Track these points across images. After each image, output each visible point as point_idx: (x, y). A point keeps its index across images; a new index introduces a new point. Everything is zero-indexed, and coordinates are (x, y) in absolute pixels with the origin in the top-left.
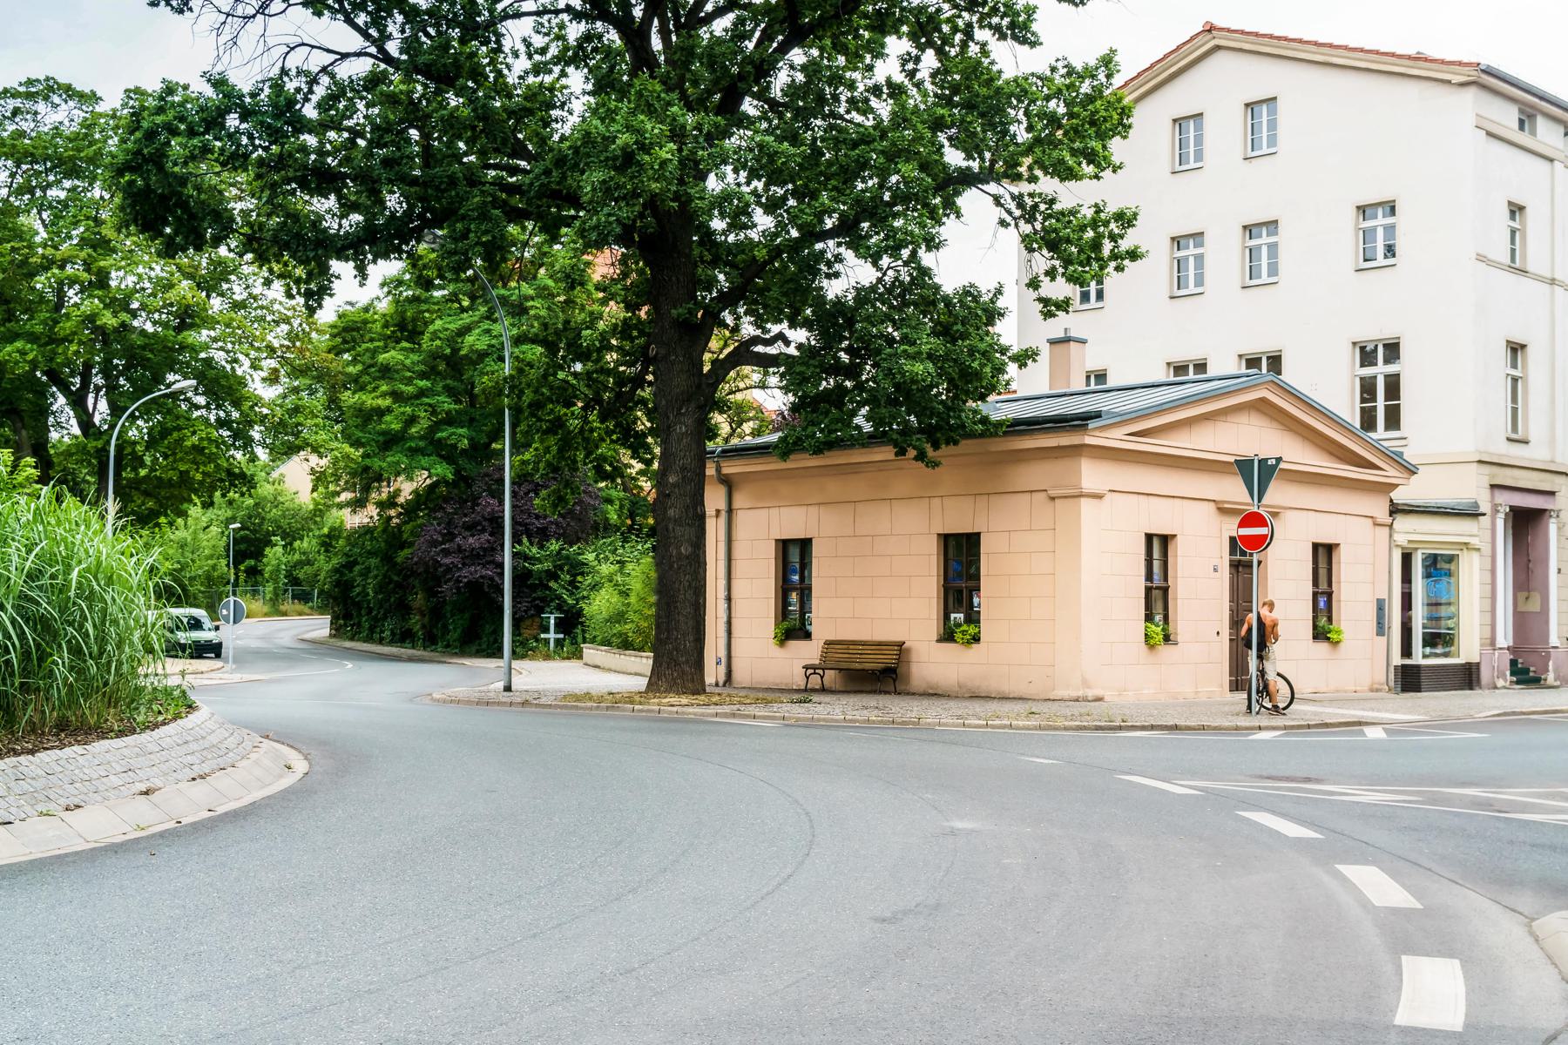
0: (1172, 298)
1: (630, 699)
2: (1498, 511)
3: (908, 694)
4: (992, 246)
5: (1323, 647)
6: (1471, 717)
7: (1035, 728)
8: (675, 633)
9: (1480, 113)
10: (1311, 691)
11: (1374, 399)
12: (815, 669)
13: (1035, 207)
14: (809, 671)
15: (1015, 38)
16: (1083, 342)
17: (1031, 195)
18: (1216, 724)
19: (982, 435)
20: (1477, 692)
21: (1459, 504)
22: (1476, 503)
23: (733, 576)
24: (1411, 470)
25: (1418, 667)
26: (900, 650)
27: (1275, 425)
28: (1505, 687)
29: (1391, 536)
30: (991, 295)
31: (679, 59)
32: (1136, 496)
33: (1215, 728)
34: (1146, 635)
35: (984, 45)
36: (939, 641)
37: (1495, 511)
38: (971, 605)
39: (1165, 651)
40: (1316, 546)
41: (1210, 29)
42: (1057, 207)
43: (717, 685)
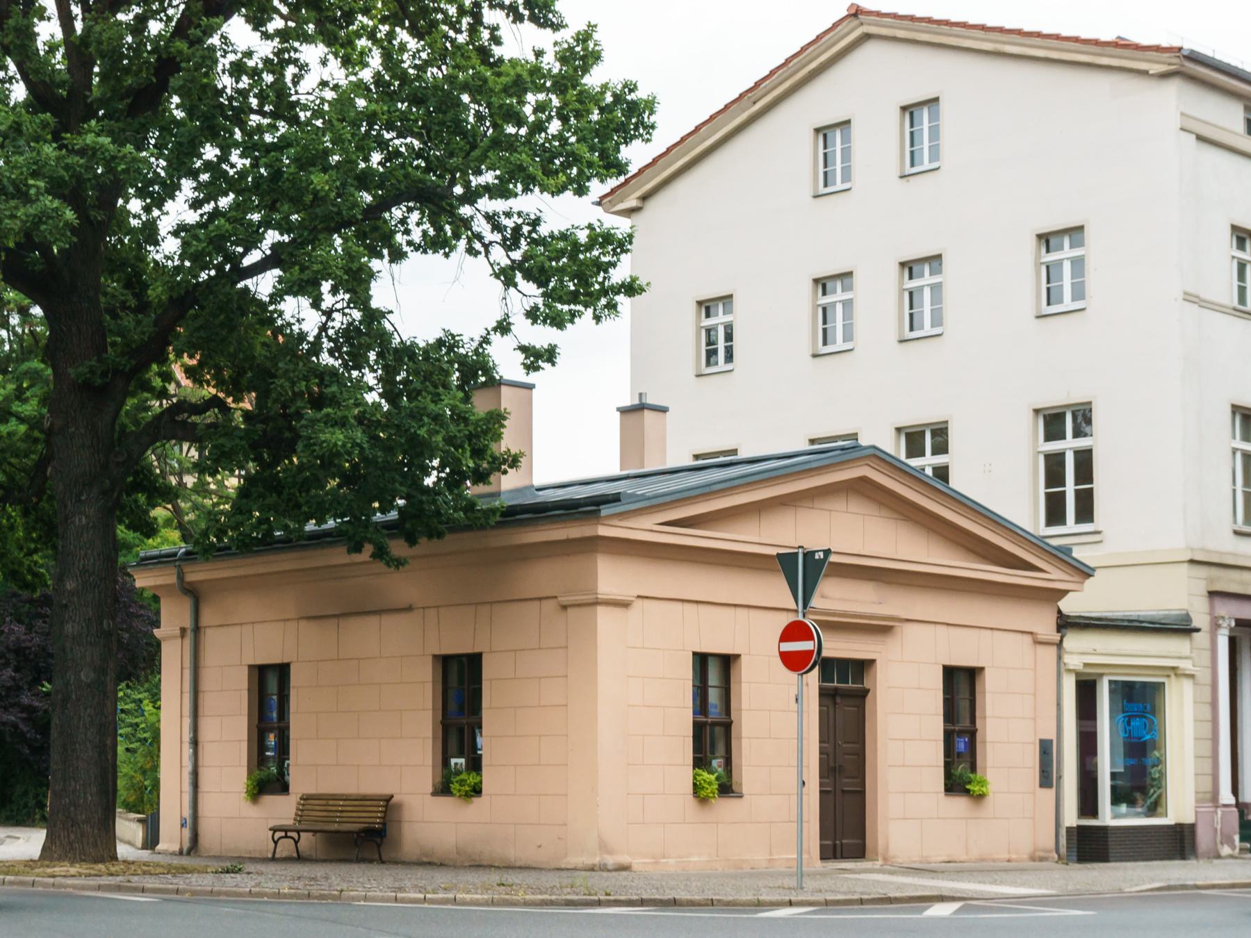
0: (815, 356)
1: (30, 864)
2: (1219, 626)
3: (396, 862)
4: (457, 279)
5: (959, 804)
6: (1121, 891)
7: (486, 903)
8: (73, 783)
9: (1187, 111)
10: (940, 859)
11: (1062, 483)
12: (286, 831)
13: (517, 229)
14: (278, 835)
15: (534, 19)
16: (663, 410)
17: (508, 215)
18: (731, 898)
19: (468, 528)
20: (1192, 862)
21: (1166, 616)
22: (1188, 615)
23: (201, 712)
24: (1085, 572)
25: (1104, 830)
26: (386, 806)
27: (885, 513)
28: (1231, 857)
29: (1059, 658)
30: (475, 344)
31: (11, 42)
32: (679, 606)
33: (728, 904)
34: (695, 784)
35: (494, 29)
36: (434, 794)
37: (1215, 625)
38: (474, 747)
39: (726, 807)
40: (701, 660)
41: (856, 13)
42: (544, 230)
43: (181, 853)
